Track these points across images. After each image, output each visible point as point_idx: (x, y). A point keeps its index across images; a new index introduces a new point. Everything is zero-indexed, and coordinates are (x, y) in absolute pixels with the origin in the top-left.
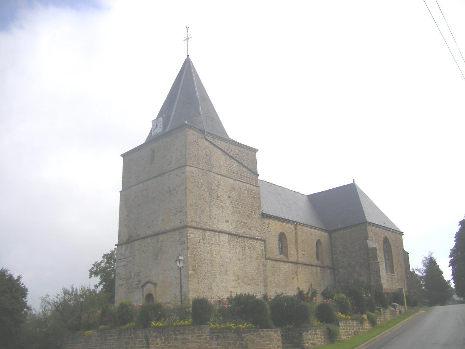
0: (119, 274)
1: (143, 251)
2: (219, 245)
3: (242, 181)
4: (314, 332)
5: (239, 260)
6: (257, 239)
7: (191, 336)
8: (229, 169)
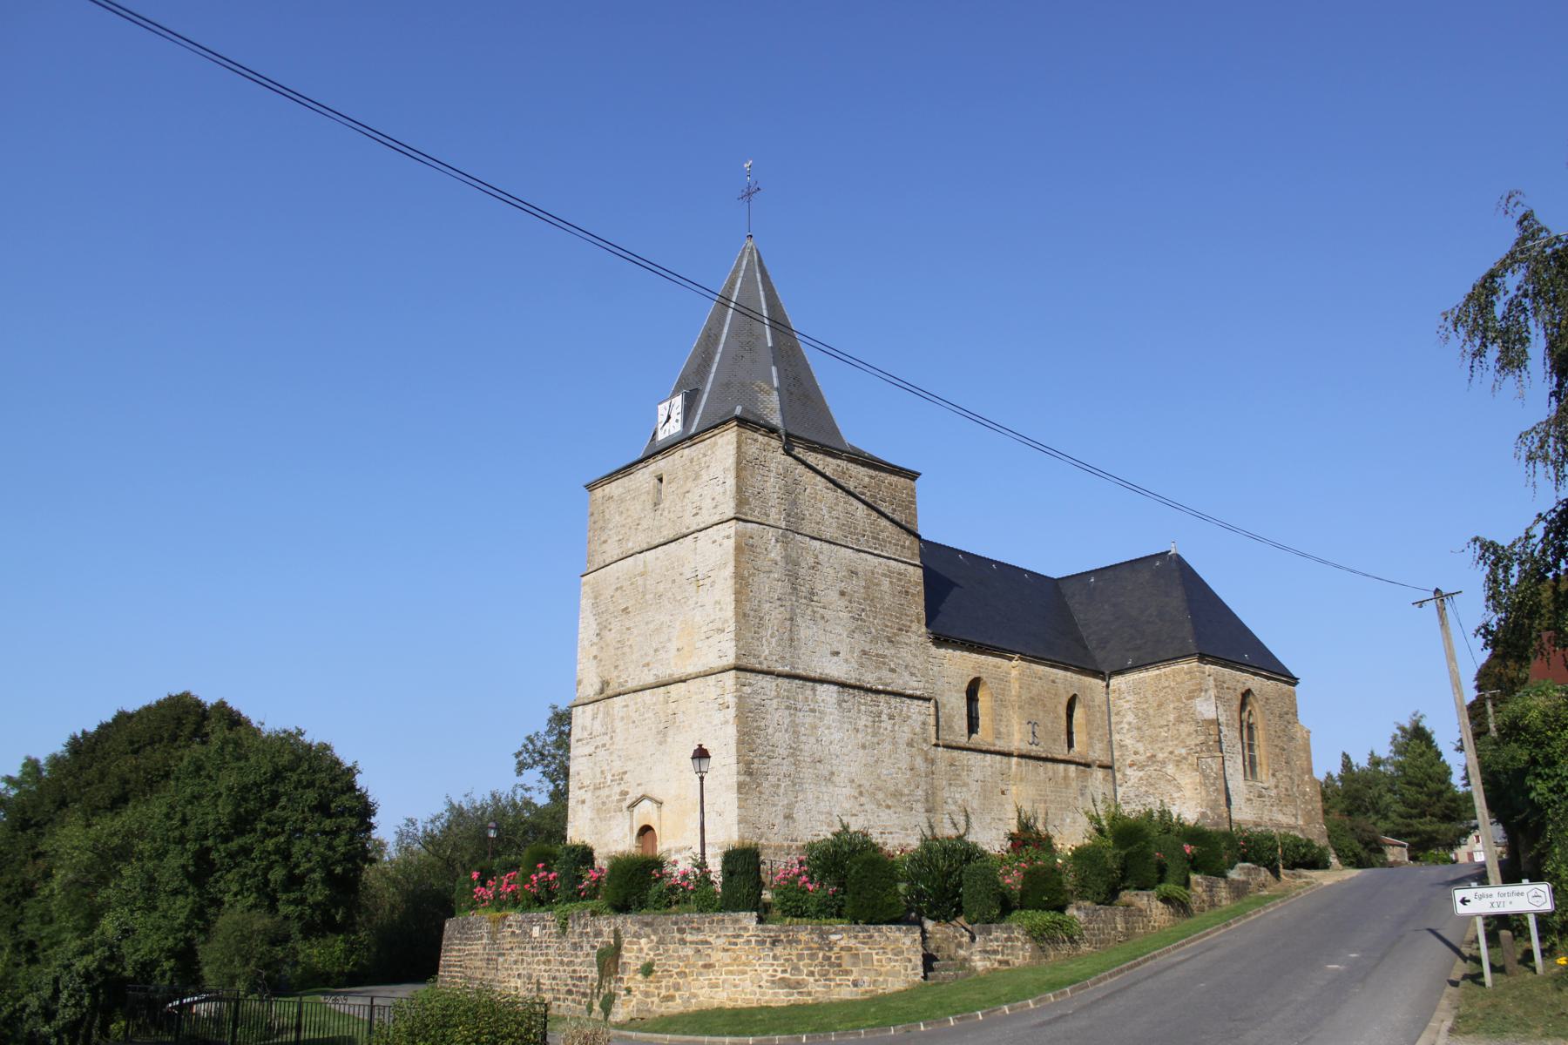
0: (578, 774)
1: (634, 722)
2: (813, 711)
3: (876, 552)
4: (1005, 935)
5: (864, 747)
6: (911, 697)
7: (715, 935)
8: (843, 525)
